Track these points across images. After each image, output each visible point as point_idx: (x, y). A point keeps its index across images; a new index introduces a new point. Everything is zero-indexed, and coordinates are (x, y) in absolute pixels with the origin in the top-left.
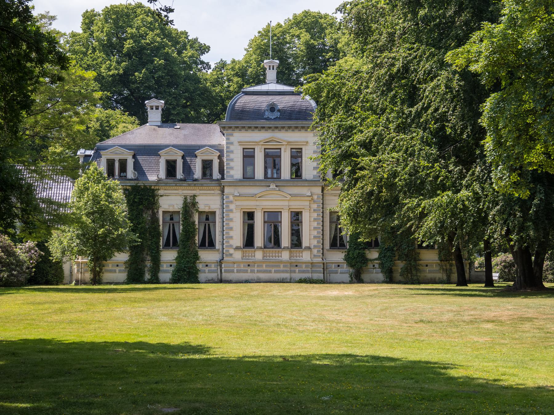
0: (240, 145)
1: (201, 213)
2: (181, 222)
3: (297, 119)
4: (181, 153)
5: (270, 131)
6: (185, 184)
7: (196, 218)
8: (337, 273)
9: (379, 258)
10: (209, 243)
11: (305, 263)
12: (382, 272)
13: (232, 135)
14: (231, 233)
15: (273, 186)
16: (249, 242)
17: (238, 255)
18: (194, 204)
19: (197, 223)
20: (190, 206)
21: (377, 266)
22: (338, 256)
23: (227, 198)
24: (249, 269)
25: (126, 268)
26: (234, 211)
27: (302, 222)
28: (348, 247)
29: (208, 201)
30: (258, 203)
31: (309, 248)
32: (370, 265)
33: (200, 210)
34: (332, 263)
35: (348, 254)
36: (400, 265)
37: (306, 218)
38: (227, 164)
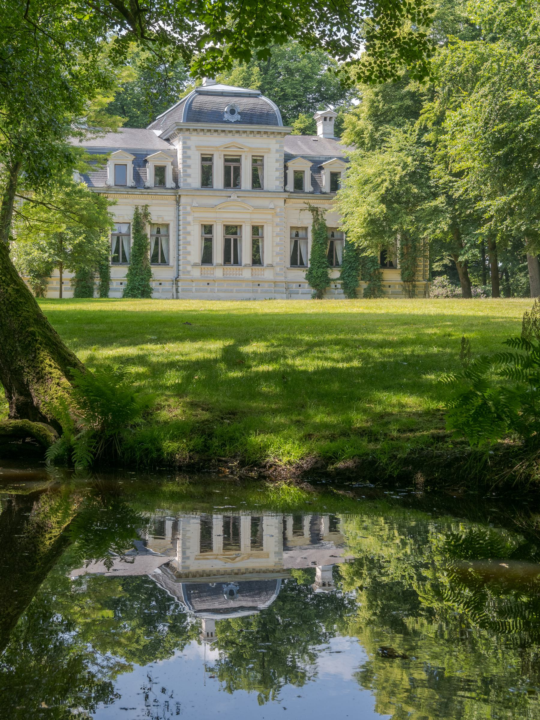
0: (197, 150)
1: (152, 225)
2: (132, 235)
3: (258, 123)
6: (137, 191)
7: (148, 230)
8: (298, 293)
9: (342, 278)
10: (159, 258)
11: (269, 282)
12: (344, 293)
13: (189, 139)
14: (189, 248)
17: (196, 273)
18: (146, 215)
19: (149, 236)
20: (140, 220)
21: (339, 286)
22: (300, 274)
23: (185, 208)
24: (209, 288)
25: (73, 285)
26: (192, 223)
27: (263, 237)
28: (309, 266)
29: (161, 210)
32: (332, 285)
33: (152, 222)
34: (266, 282)
35: (310, 272)
36: (364, 285)
37: (268, 233)
38: (185, 171)
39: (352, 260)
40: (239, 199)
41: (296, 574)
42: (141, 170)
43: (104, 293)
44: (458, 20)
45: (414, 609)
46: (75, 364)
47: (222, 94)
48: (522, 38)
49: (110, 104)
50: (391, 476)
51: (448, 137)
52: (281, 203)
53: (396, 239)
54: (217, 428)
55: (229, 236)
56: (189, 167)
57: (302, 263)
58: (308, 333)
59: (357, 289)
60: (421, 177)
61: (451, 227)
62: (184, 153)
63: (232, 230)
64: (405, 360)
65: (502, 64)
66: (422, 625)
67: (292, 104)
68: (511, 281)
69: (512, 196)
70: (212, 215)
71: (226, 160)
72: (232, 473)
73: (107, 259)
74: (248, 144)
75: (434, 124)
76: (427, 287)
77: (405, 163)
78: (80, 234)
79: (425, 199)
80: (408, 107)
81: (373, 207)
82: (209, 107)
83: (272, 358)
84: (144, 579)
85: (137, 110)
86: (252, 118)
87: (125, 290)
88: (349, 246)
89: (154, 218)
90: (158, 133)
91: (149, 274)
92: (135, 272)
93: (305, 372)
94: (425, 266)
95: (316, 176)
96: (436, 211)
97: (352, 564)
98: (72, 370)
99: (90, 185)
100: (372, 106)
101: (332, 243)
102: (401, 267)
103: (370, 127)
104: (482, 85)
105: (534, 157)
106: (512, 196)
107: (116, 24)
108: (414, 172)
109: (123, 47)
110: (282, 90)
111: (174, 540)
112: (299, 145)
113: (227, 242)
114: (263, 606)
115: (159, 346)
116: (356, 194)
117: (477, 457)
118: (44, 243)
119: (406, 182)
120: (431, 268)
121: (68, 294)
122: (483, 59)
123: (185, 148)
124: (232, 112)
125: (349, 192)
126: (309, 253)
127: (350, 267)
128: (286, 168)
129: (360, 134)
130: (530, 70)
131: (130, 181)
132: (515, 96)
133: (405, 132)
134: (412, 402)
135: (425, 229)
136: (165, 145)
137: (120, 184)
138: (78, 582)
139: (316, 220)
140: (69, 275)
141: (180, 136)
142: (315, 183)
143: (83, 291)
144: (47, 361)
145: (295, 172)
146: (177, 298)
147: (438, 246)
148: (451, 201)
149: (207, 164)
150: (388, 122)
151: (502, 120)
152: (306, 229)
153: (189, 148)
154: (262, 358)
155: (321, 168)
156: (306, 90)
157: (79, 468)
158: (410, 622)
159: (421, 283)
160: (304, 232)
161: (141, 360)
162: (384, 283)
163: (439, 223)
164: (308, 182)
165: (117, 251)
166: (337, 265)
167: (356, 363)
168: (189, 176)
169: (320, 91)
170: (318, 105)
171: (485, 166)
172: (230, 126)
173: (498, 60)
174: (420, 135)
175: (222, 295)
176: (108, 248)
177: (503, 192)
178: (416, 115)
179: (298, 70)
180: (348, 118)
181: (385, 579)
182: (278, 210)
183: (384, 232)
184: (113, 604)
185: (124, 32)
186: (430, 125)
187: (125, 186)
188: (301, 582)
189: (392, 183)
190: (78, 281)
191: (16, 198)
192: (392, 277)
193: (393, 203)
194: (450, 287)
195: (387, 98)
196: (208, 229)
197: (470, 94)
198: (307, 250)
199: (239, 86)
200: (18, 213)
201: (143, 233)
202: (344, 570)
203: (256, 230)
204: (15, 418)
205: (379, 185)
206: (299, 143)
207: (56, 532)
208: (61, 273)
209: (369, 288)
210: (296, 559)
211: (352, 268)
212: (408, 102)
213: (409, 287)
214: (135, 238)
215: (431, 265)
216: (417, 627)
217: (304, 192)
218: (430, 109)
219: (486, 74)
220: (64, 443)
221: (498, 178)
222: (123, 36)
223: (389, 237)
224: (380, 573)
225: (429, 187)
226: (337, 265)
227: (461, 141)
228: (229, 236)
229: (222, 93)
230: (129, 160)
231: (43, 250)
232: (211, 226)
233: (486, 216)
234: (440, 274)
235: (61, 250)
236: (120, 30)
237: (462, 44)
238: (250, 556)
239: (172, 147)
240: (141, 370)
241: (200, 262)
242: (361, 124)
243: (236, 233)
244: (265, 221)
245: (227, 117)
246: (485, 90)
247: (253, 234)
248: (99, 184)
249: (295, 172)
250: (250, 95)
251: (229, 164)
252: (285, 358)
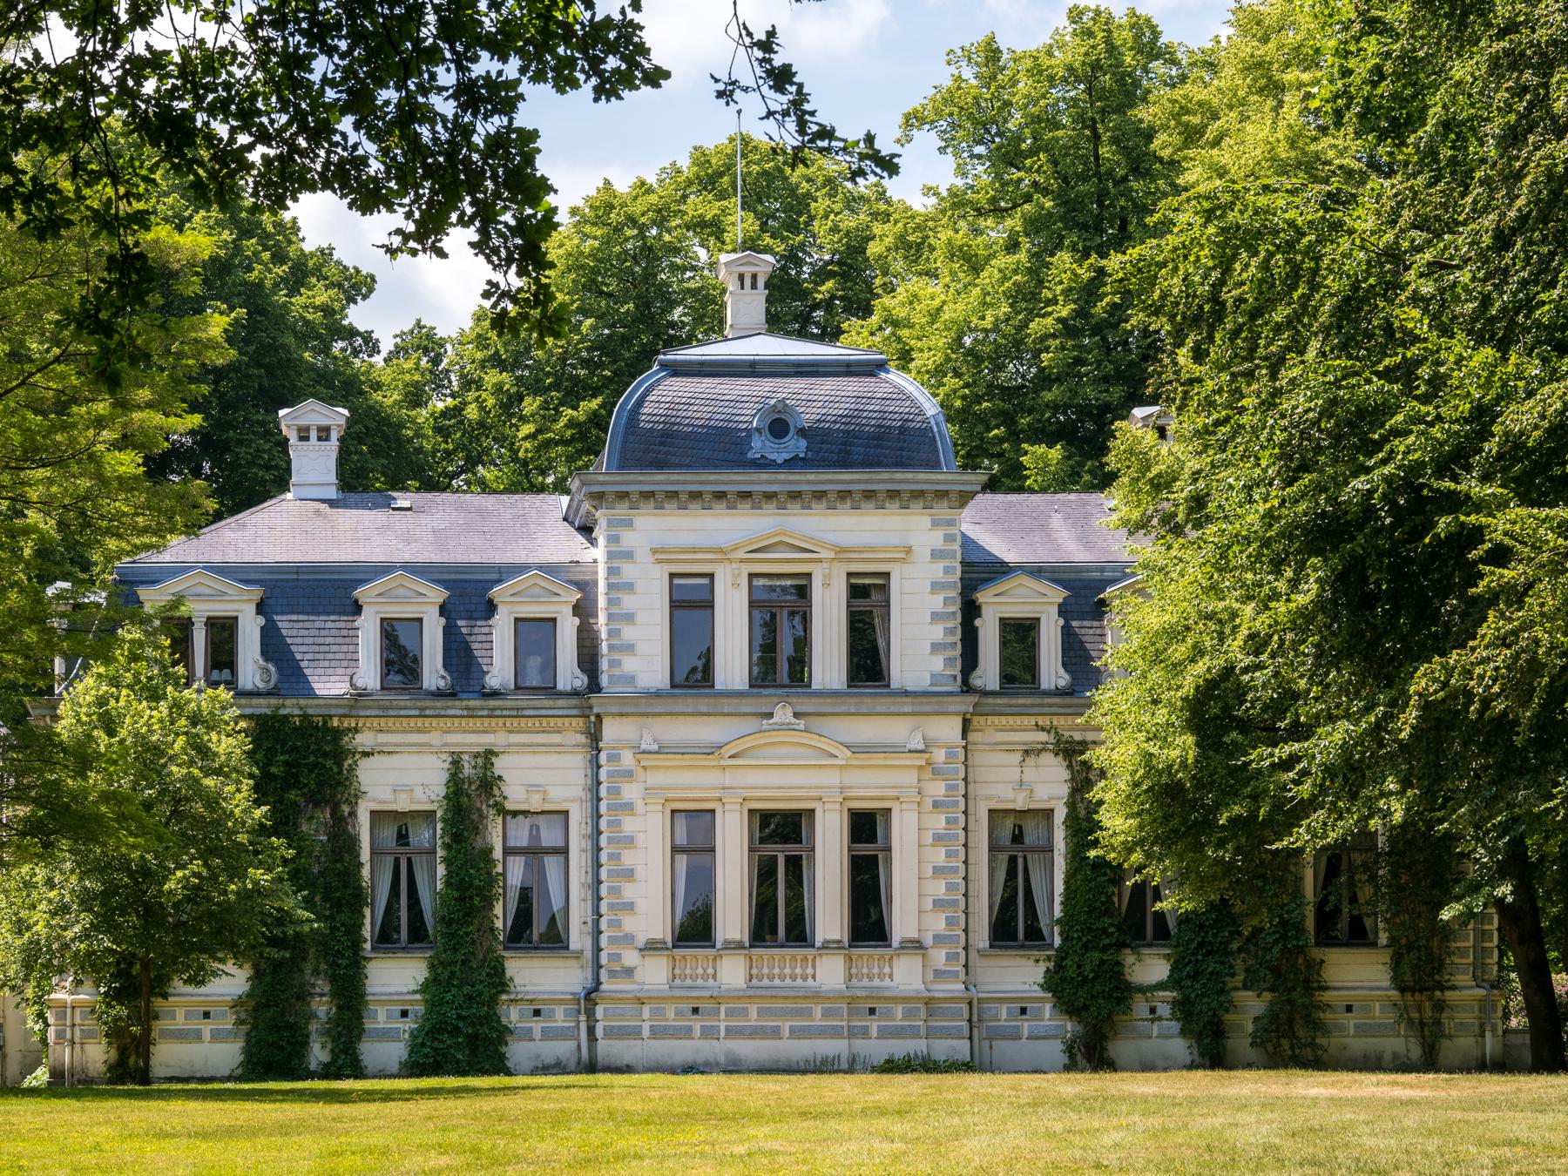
0: (659, 561)
2: (440, 853)
3: (869, 463)
6: (455, 707)
9: (1173, 982)
10: (537, 930)
11: (905, 1000)
13: (629, 524)
14: (630, 891)
15: (783, 714)
17: (654, 973)
18: (489, 784)
19: (498, 854)
21: (1164, 1010)
22: (1022, 975)
23: (614, 758)
25: (240, 1022)
26: (640, 807)
28: (1057, 941)
29: (539, 770)
30: (728, 779)
31: (916, 946)
32: (1140, 1007)
33: (509, 806)
35: (1059, 967)
36: (1251, 1005)
40: (801, 724)
52: (950, 729)
55: (771, 849)
59: (1228, 1017)
63: (781, 830)
82: (700, 414)
89: (515, 794)
91: (499, 981)
92: (447, 974)
102: (1393, 941)
113: (764, 874)
126: (1058, 900)
127: (1200, 946)
128: (970, 610)
131: (433, 672)
152: (1048, 814)
153: (629, 555)
160: (1042, 824)
162: (1328, 996)
172: (765, 477)
173: (1290, 245)
187: (550, 691)
190: (256, 1009)
198: (1054, 884)
213: (1419, 1009)
214: (448, 861)
229: (753, 364)
241: (669, 939)
244: (893, 793)
245: (760, 446)
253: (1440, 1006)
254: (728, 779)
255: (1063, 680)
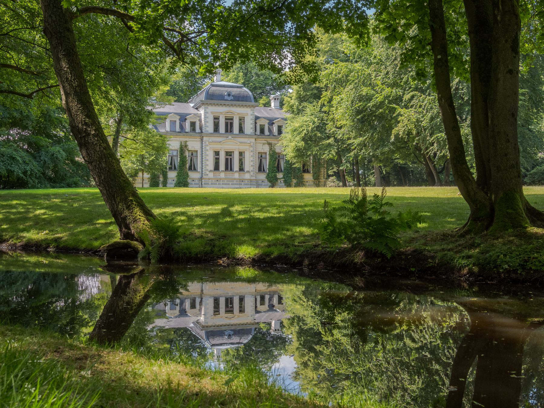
4: (179, 117)
5: (228, 107)
6: (181, 134)
7: (187, 154)
9: (284, 178)
10: (193, 168)
15: (230, 137)
16: (217, 167)
17: (211, 175)
18: (186, 146)
20: (183, 149)
21: (282, 182)
22: (263, 176)
29: (193, 144)
30: (222, 146)
31: (248, 172)
32: (279, 181)
35: (268, 175)
36: (294, 181)
39: (289, 169)
41: (262, 326)
42: (183, 124)
43: (165, 185)
44: (338, 52)
45: (320, 342)
46: (152, 215)
47: (224, 86)
48: (369, 61)
49: (168, 90)
50: (294, 262)
51: (334, 109)
52: (253, 140)
53: (310, 159)
54: (217, 243)
55: (227, 157)
56: (207, 122)
57: (264, 170)
58: (263, 202)
60: (322, 128)
61: (336, 153)
62: (205, 115)
63: (229, 154)
64: (305, 213)
65: (360, 74)
66: (324, 349)
67: (259, 91)
68: (367, 179)
69: (365, 138)
70: (220, 146)
71: (226, 119)
72: (223, 263)
73: (166, 168)
74: (238, 111)
75: (328, 102)
76: (325, 182)
77: (314, 121)
78: (153, 155)
79: (324, 139)
80: (315, 94)
81: (298, 143)
82: (217, 92)
83: (245, 212)
84: (186, 330)
85: (181, 95)
86: (240, 99)
87: (175, 184)
88: (287, 162)
90: (192, 105)
93: (259, 218)
94: (324, 172)
95: (271, 127)
96: (329, 145)
97: (289, 319)
98: (150, 218)
99: (158, 131)
100: (297, 93)
101: (279, 160)
103: (297, 103)
104: (350, 84)
105: (376, 119)
106: (365, 138)
107: (171, 54)
108: (318, 126)
109: (174, 65)
110: (254, 84)
111: (200, 310)
112: (261, 112)
113: (227, 160)
114: (245, 341)
115: (191, 208)
116: (290, 136)
117: (331, 253)
118: (134, 159)
119: (314, 131)
120: (327, 173)
121: (147, 185)
122: (351, 71)
123: (206, 113)
124: (229, 95)
125: (287, 135)
128: (256, 123)
129: (292, 107)
130: (373, 77)
131: (178, 129)
132: (365, 91)
133: (314, 106)
134: (306, 230)
135: (324, 154)
136: (195, 111)
137: (173, 131)
138: (152, 331)
139: (271, 149)
140: (147, 176)
141: (203, 107)
142: (270, 131)
143: (154, 183)
144: (138, 213)
145: (260, 125)
146: (202, 187)
147: (330, 162)
148: (336, 140)
149: (216, 121)
150: (306, 101)
151: (360, 101)
152: (266, 153)
153: (207, 113)
154: (240, 213)
155: (273, 123)
156: (266, 84)
157: (153, 261)
158: (318, 348)
159: (322, 180)
161: (183, 214)
163: (331, 151)
164: (267, 130)
165: (171, 164)
166: (281, 171)
167: (282, 215)
168: (207, 127)
169: (273, 85)
170: (272, 92)
171: (352, 123)
173: (358, 72)
174: (321, 108)
175: (224, 186)
176: (167, 163)
177: (361, 135)
178: (319, 98)
179: (262, 75)
180: (286, 99)
181: (306, 327)
182: (252, 144)
183: (304, 155)
184: (170, 342)
185: (174, 59)
186: (326, 103)
188: (265, 330)
189: (308, 131)
191: (120, 137)
192: (308, 177)
193: (308, 141)
194: (337, 182)
195: (305, 90)
196: (217, 153)
197: (344, 88)
198: (267, 164)
199: (233, 82)
200: (121, 145)
201: (185, 155)
202: (286, 323)
203: (241, 154)
204: (123, 239)
205: (301, 132)
206: (262, 111)
207: (142, 293)
208: (143, 174)
209: (297, 182)
210: (262, 318)
211: (289, 173)
212: (315, 91)
214: (180, 157)
215: (327, 172)
216: (321, 349)
217: (265, 135)
218: (326, 95)
219: (352, 79)
220: (146, 251)
221: (359, 129)
222: (174, 61)
223: (307, 158)
224: (303, 323)
225: (326, 133)
226: (281, 171)
227: (341, 110)
228: (227, 157)
230: (177, 119)
231: (134, 163)
232: (219, 152)
233: (353, 148)
234: (332, 176)
235: (143, 163)
236: (173, 58)
237: (341, 64)
238: (239, 317)
239: (199, 112)
240: (183, 218)
242: (292, 102)
243: (231, 155)
246: (351, 86)
247: (240, 156)
248: (162, 130)
249: (260, 125)
250: (238, 87)
251: (227, 121)
252: (251, 212)
253: (319, 182)
254: (222, 146)
255: (268, 134)
